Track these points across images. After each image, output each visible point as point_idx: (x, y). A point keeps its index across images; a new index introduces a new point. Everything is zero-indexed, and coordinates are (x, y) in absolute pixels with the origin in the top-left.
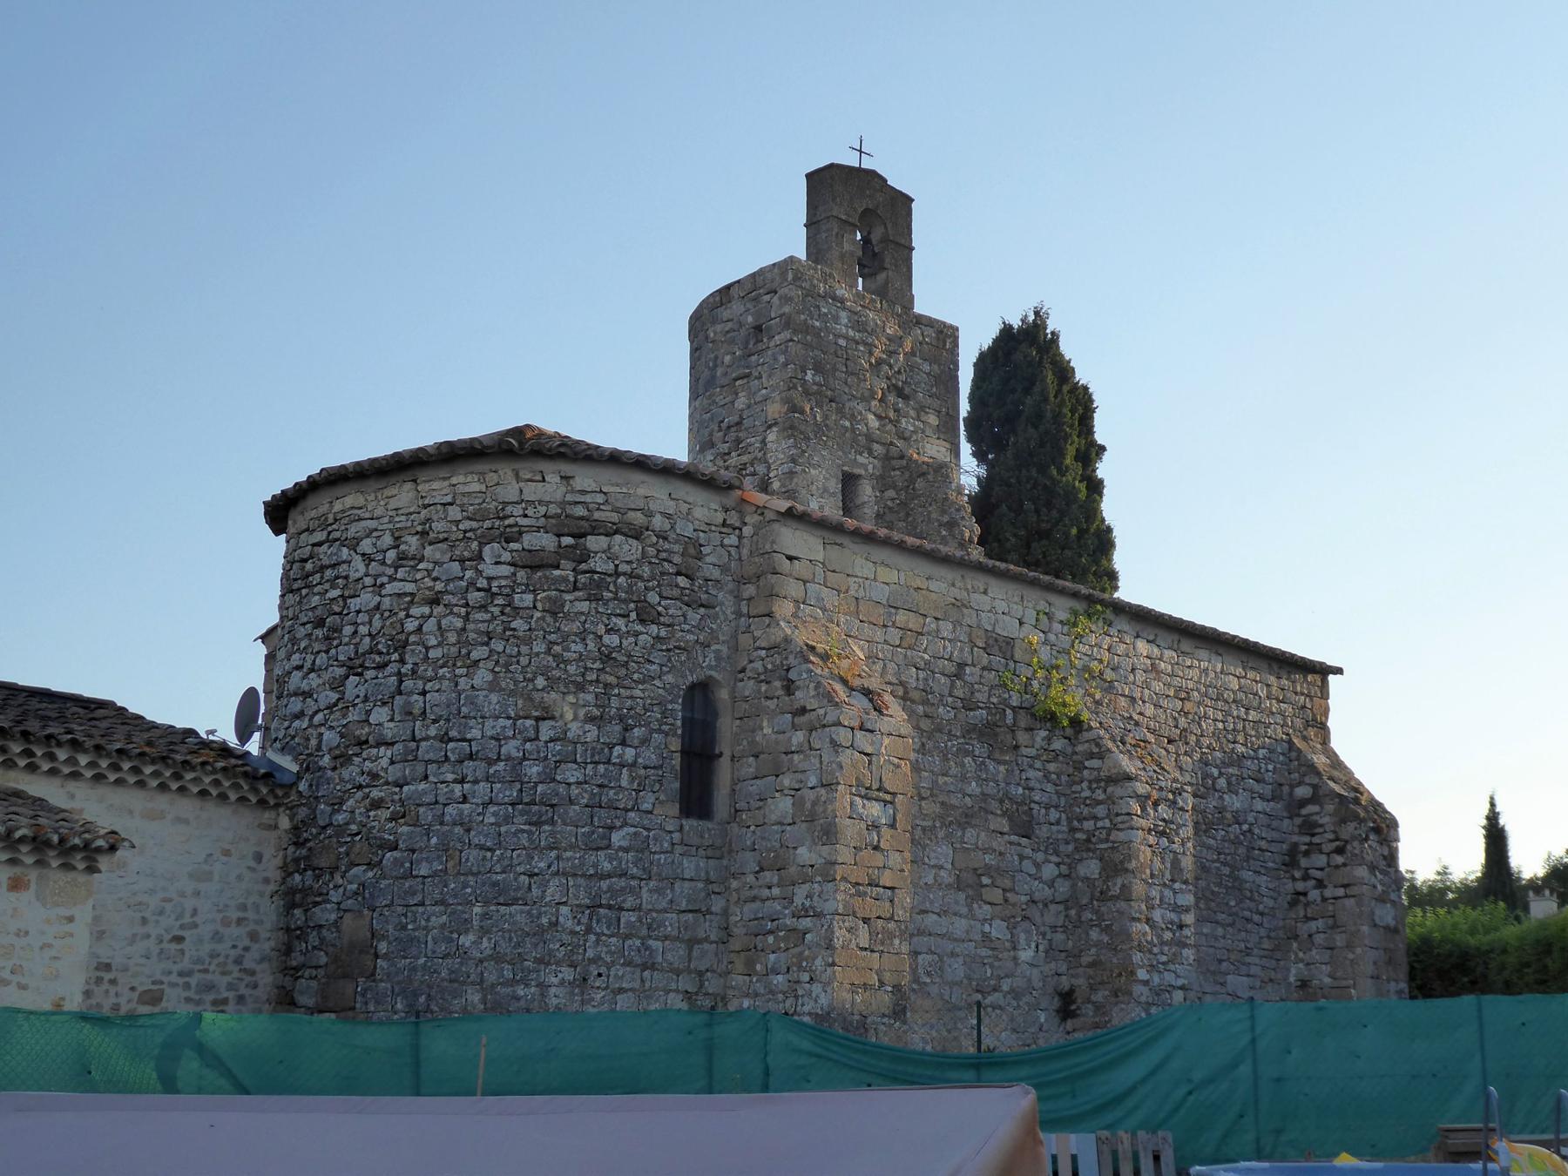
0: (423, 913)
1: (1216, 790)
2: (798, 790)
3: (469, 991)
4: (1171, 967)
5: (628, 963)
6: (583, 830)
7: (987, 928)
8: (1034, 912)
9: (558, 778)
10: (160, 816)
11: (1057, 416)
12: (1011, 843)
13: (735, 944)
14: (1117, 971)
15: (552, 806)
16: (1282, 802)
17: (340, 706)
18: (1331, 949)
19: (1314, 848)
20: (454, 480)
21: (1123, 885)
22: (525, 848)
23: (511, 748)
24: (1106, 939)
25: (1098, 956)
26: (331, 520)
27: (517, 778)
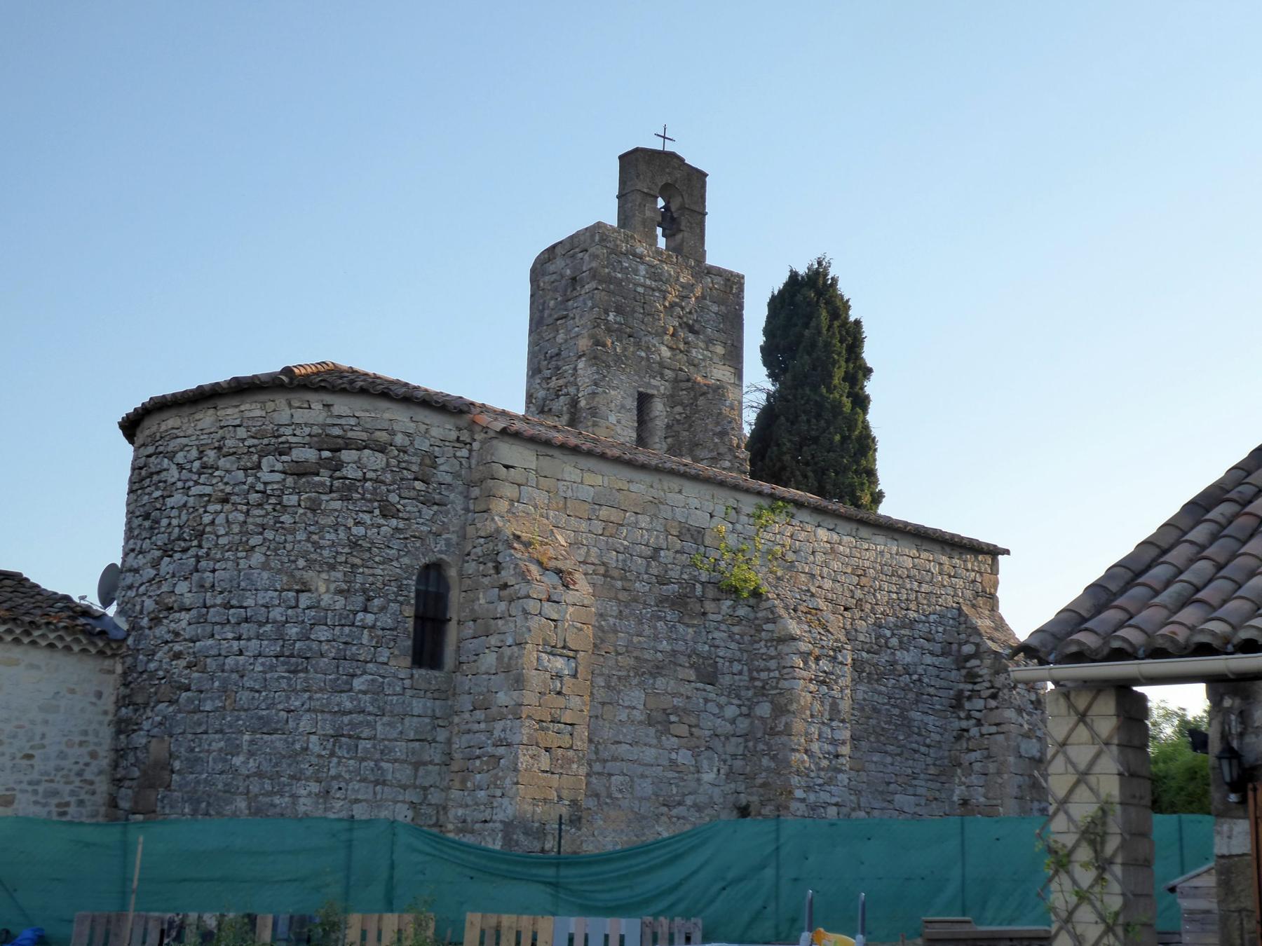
0: (206, 739)
1: (889, 648)
2: (500, 647)
3: (238, 800)
4: (827, 788)
5: (363, 780)
6: (330, 677)
7: (674, 756)
8: (717, 744)
9: (312, 637)
10: (16, 663)
11: (827, 345)
12: (697, 689)
13: (455, 767)
14: (779, 790)
15: (307, 658)
16: (951, 657)
17: (157, 580)
18: (986, 774)
19: (975, 694)
20: (242, 408)
21: (787, 723)
22: (284, 691)
23: (276, 614)
24: (773, 765)
25: (767, 778)
26: (158, 438)
27: (281, 637)
